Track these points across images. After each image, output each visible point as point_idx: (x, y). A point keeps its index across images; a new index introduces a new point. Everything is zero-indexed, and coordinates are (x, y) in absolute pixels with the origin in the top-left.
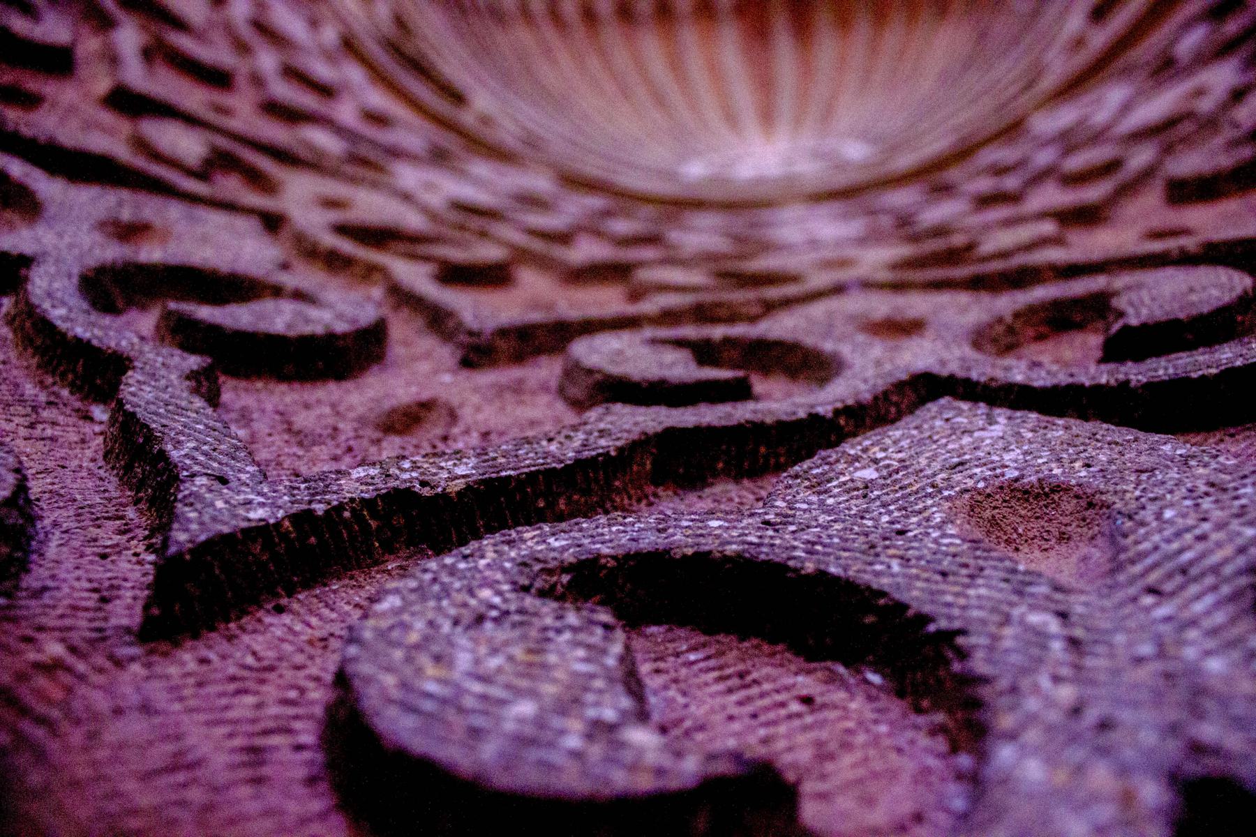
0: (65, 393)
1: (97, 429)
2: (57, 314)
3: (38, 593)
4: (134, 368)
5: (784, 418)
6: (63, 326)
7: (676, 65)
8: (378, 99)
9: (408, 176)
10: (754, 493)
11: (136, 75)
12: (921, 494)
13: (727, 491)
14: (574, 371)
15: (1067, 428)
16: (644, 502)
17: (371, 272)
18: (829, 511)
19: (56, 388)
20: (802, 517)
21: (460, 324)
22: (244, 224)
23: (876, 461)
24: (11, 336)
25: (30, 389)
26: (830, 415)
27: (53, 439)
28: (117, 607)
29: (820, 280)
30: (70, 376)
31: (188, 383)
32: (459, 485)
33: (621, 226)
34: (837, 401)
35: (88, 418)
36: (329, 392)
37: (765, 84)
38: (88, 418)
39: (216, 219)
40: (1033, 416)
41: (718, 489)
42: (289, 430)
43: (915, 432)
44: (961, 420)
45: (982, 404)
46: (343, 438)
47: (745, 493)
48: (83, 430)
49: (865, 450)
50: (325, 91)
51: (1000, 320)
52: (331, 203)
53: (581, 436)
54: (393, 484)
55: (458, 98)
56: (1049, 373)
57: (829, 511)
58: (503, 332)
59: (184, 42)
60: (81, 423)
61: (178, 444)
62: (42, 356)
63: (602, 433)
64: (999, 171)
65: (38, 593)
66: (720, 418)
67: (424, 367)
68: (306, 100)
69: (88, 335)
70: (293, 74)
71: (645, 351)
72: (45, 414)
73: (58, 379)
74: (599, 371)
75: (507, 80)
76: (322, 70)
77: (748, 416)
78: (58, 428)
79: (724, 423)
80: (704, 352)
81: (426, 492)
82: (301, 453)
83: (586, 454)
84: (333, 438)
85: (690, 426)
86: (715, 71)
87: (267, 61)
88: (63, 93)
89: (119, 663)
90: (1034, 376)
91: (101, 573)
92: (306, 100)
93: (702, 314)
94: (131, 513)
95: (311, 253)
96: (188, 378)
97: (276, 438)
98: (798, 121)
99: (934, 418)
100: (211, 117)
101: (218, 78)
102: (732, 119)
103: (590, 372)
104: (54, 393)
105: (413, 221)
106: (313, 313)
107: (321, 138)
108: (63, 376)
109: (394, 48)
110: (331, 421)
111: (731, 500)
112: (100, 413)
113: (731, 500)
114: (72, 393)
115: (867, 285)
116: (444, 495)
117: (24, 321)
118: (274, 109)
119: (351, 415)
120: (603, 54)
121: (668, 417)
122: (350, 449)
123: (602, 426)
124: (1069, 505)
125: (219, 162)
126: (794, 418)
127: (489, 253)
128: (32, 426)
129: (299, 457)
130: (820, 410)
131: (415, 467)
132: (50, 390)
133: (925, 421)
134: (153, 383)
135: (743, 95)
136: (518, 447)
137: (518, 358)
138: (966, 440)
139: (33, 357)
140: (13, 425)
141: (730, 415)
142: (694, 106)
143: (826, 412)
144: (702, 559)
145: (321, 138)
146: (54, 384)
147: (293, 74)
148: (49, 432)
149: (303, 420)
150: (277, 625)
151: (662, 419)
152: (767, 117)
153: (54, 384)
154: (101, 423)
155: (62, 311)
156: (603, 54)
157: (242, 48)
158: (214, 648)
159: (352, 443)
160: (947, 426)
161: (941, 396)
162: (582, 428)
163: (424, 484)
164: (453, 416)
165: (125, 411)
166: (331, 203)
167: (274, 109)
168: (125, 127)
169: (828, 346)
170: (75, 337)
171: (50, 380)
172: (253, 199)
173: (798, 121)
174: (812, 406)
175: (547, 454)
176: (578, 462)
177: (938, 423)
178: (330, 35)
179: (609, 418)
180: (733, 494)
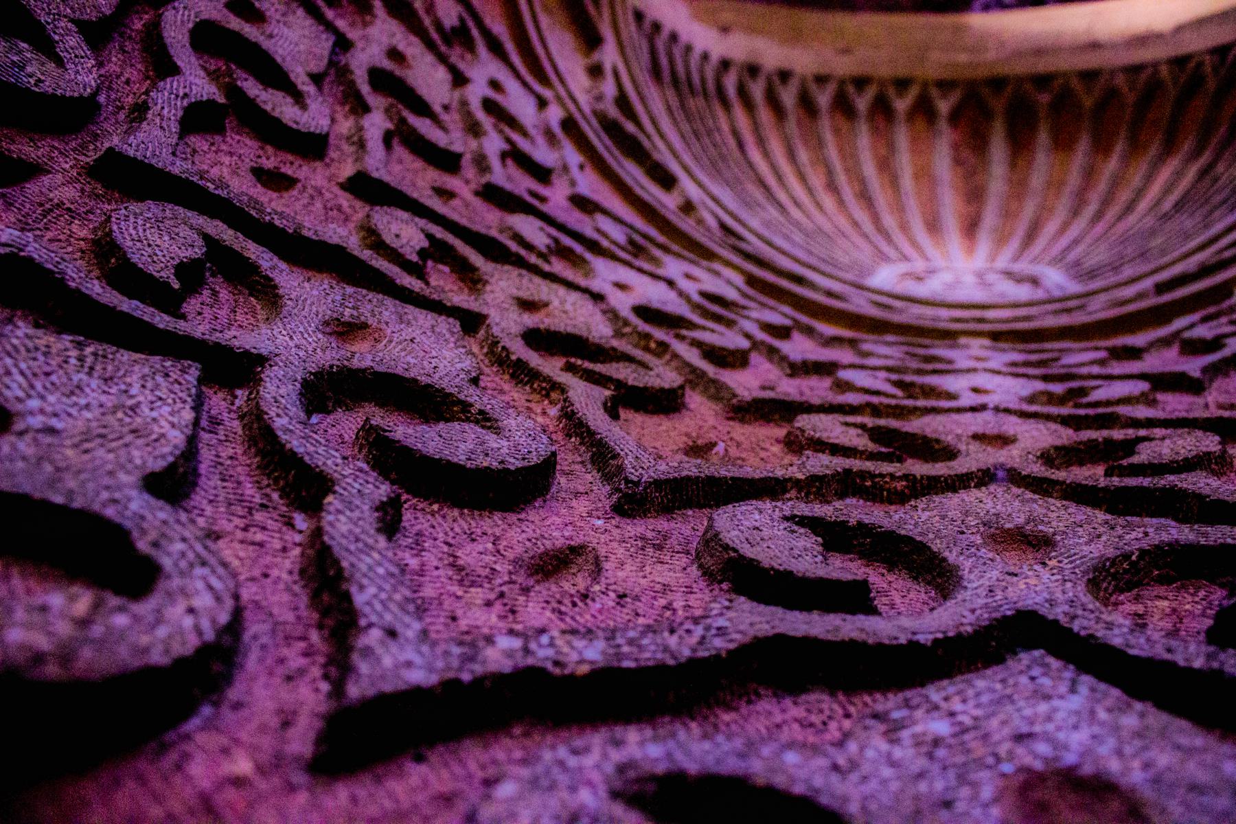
0: (275, 496)
1: (298, 538)
2: (279, 423)
3: (237, 706)
4: (335, 492)
5: (887, 642)
6: (284, 437)
7: (886, 165)
8: (589, 184)
9: (604, 274)
10: (844, 708)
11: (377, 162)
12: (980, 764)
13: (819, 701)
14: (711, 541)
15: (1142, 715)
16: (745, 699)
17: (551, 388)
18: (893, 764)
19: (268, 490)
20: (866, 768)
21: (621, 469)
22: (445, 325)
23: (952, 714)
24: (240, 432)
25: (249, 490)
26: (929, 644)
27: (261, 545)
28: (292, 732)
29: (974, 458)
30: (282, 483)
31: (376, 514)
32: (584, 669)
33: (799, 348)
34: (939, 631)
35: (290, 524)
36: (493, 523)
37: (975, 195)
38: (290, 524)
39: (424, 319)
40: (1115, 692)
41: (813, 697)
42: (452, 565)
43: (998, 686)
44: (1046, 682)
45: (1071, 667)
46: (499, 581)
47: (836, 707)
48: (287, 537)
49: (946, 699)
50: (542, 174)
51: (1126, 556)
52: (528, 305)
53: (699, 631)
54: (530, 661)
55: (667, 181)
56: (1148, 640)
57: (893, 764)
58: (658, 484)
59: (423, 126)
60: (284, 529)
61: (362, 588)
62: (263, 458)
63: (721, 631)
64: (1193, 348)
65: (237, 706)
66: (828, 631)
67: (582, 506)
68: (521, 184)
69: (301, 450)
70: (515, 155)
71: (780, 530)
72: (259, 516)
73: (271, 482)
74: (735, 550)
75: (716, 167)
76: (542, 154)
77: (855, 635)
78: (266, 533)
79: (830, 637)
80: (876, 434)
81: (557, 671)
82: (460, 593)
83: (702, 654)
84: (490, 580)
85: (799, 634)
86: (924, 175)
87: (493, 144)
88: (313, 175)
89: (291, 788)
90: (1133, 641)
91: (286, 695)
92: (521, 184)
93: (847, 484)
94: (315, 636)
95: (500, 359)
96: (377, 509)
97: (441, 572)
98: (1001, 240)
99: (1021, 672)
100: (436, 204)
101: (448, 161)
102: (934, 226)
103: (726, 547)
104: (267, 495)
105: (599, 329)
106: (492, 441)
107: (528, 227)
108: (276, 481)
109: (611, 128)
110: (488, 558)
111: (821, 711)
112: (300, 521)
113: (821, 711)
114: (281, 497)
115: (1015, 478)
116: (572, 676)
117: (253, 423)
118: (493, 195)
119: (510, 555)
120: (818, 145)
121: (782, 620)
122: (502, 595)
123: (721, 622)
124: (1115, 805)
125: (437, 251)
126: (895, 642)
127: (664, 376)
128: (245, 529)
129: (458, 597)
130: (921, 638)
131: (552, 644)
132: (264, 491)
133: (1012, 675)
134: (348, 513)
135: (951, 205)
136: (643, 634)
137: (667, 510)
138: (1043, 708)
139: (256, 456)
140: (232, 525)
141: (837, 629)
142: (899, 208)
143: (927, 640)
144: (770, 792)
145: (528, 227)
146: (268, 486)
147: (515, 155)
148: (259, 537)
149: (469, 555)
150: (416, 773)
151: (777, 623)
152: (971, 228)
153: (268, 486)
154: (301, 532)
155: (284, 421)
156: (818, 145)
157: (474, 129)
158: (363, 788)
159: (504, 588)
160: (1031, 686)
161: (1036, 647)
162: (703, 621)
163: (557, 663)
164: (597, 571)
165: (323, 543)
166: (528, 305)
167: (493, 195)
168: (360, 210)
169: (952, 557)
170: (291, 450)
171: (265, 482)
172: (459, 298)
173: (1001, 240)
174: (914, 633)
175: (666, 649)
176: (693, 662)
177: (1024, 680)
178: (555, 114)
179: (731, 614)
180: (825, 706)
